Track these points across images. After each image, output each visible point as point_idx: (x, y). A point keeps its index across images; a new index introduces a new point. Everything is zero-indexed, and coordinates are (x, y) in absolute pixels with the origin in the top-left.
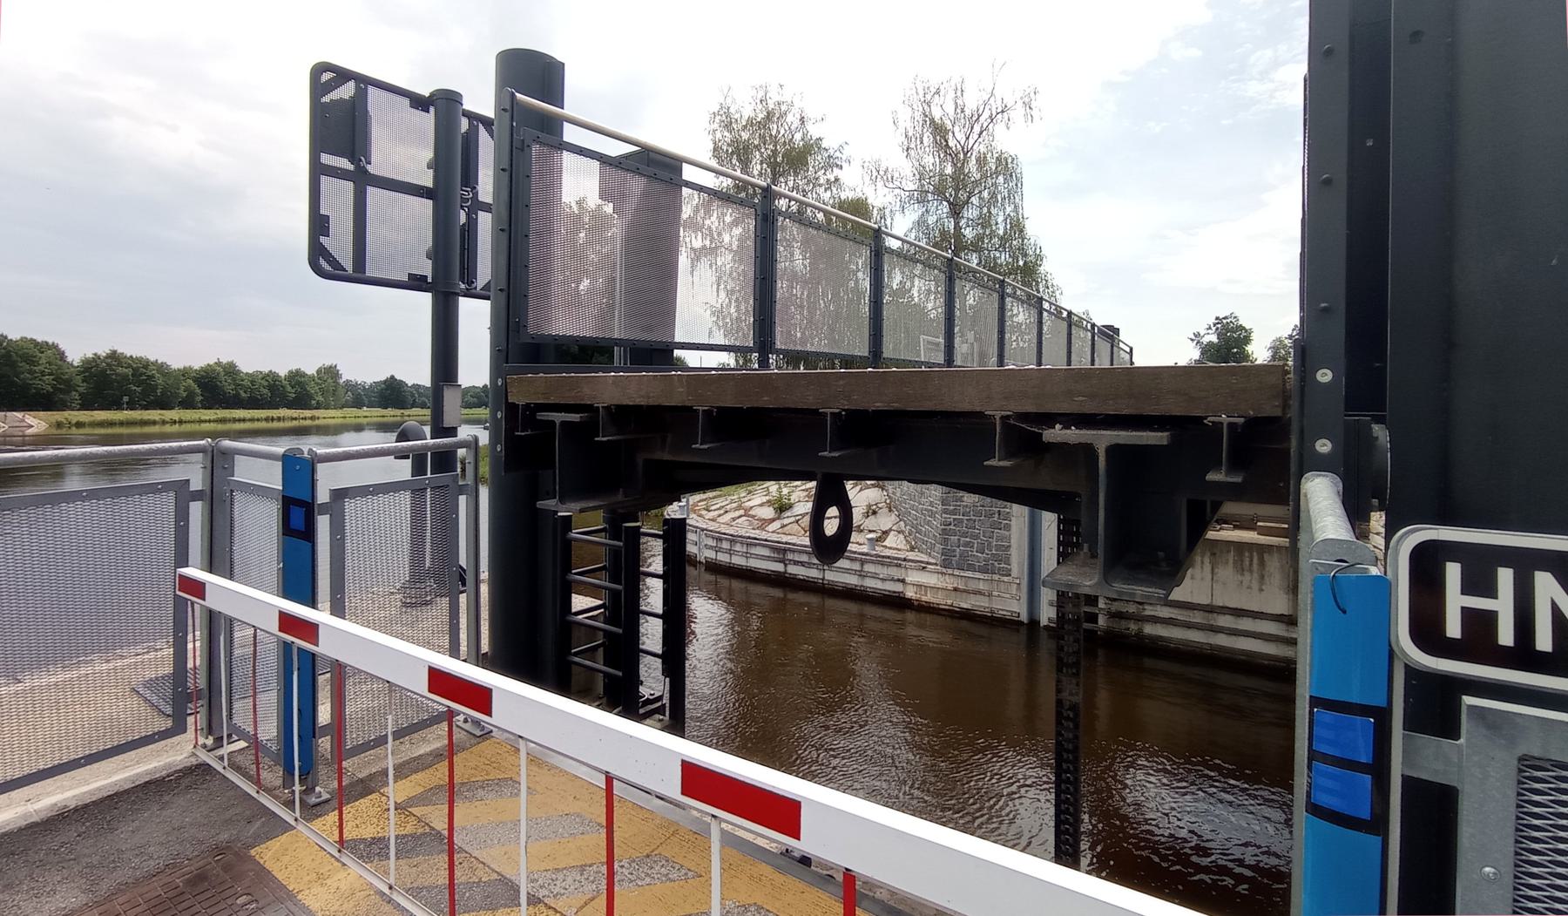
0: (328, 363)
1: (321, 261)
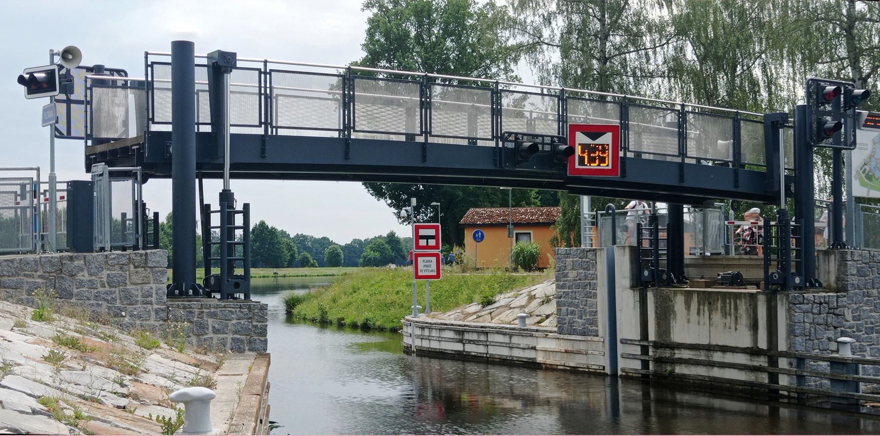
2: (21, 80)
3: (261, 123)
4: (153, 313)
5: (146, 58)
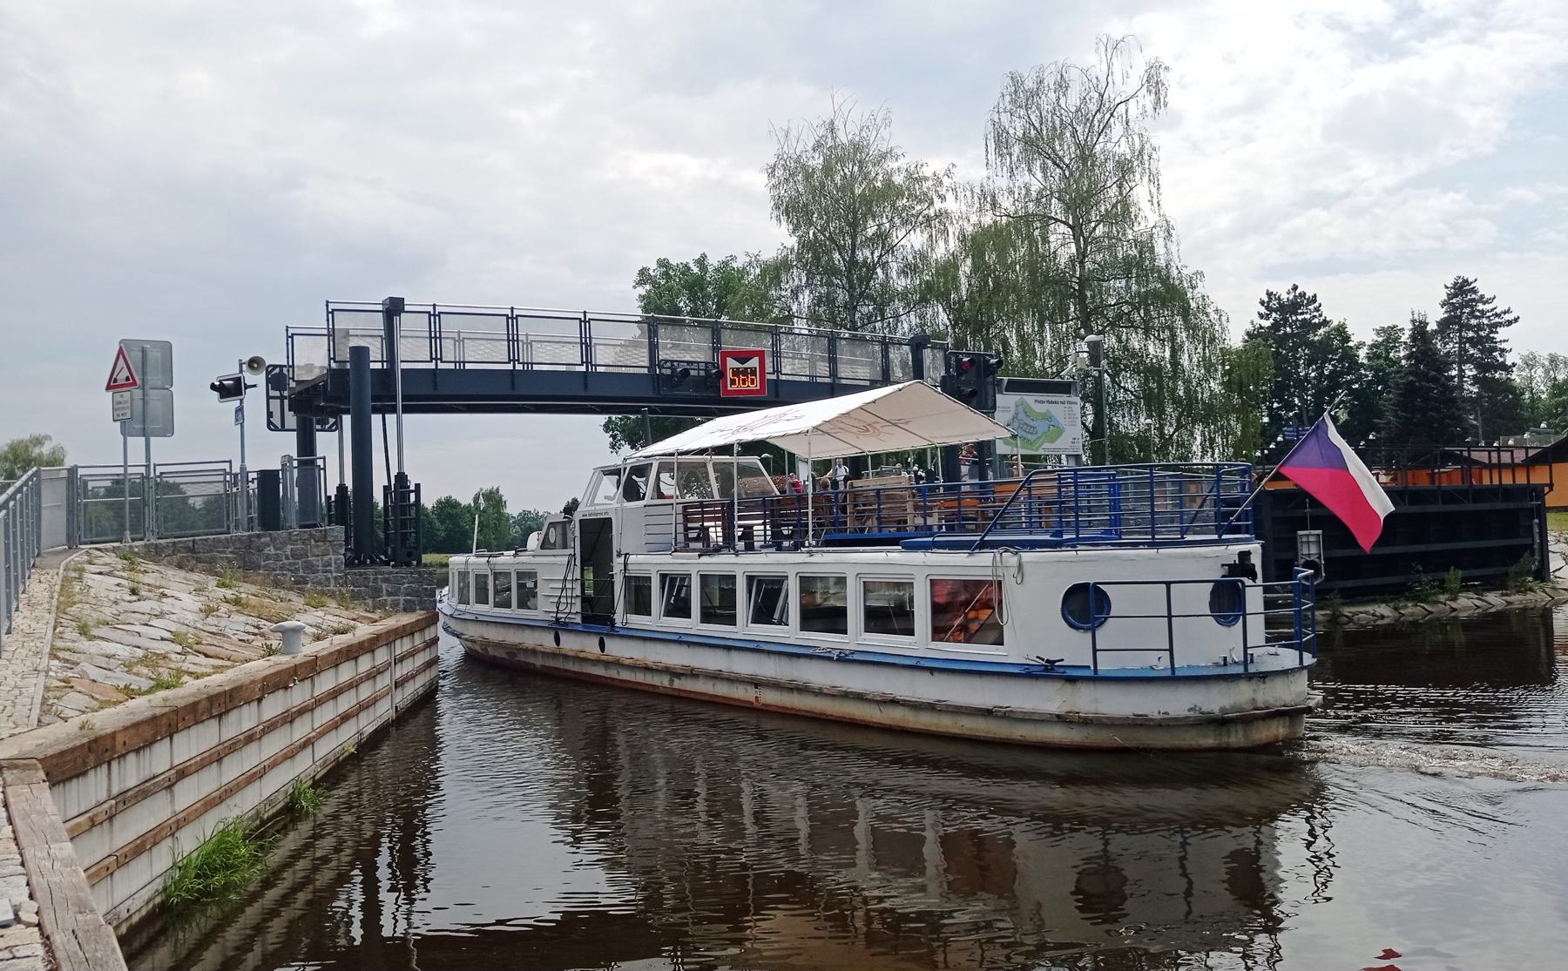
0: (487, 487)
1: (270, 425)
2: (213, 387)
3: (432, 359)
4: (332, 581)
5: (327, 306)
